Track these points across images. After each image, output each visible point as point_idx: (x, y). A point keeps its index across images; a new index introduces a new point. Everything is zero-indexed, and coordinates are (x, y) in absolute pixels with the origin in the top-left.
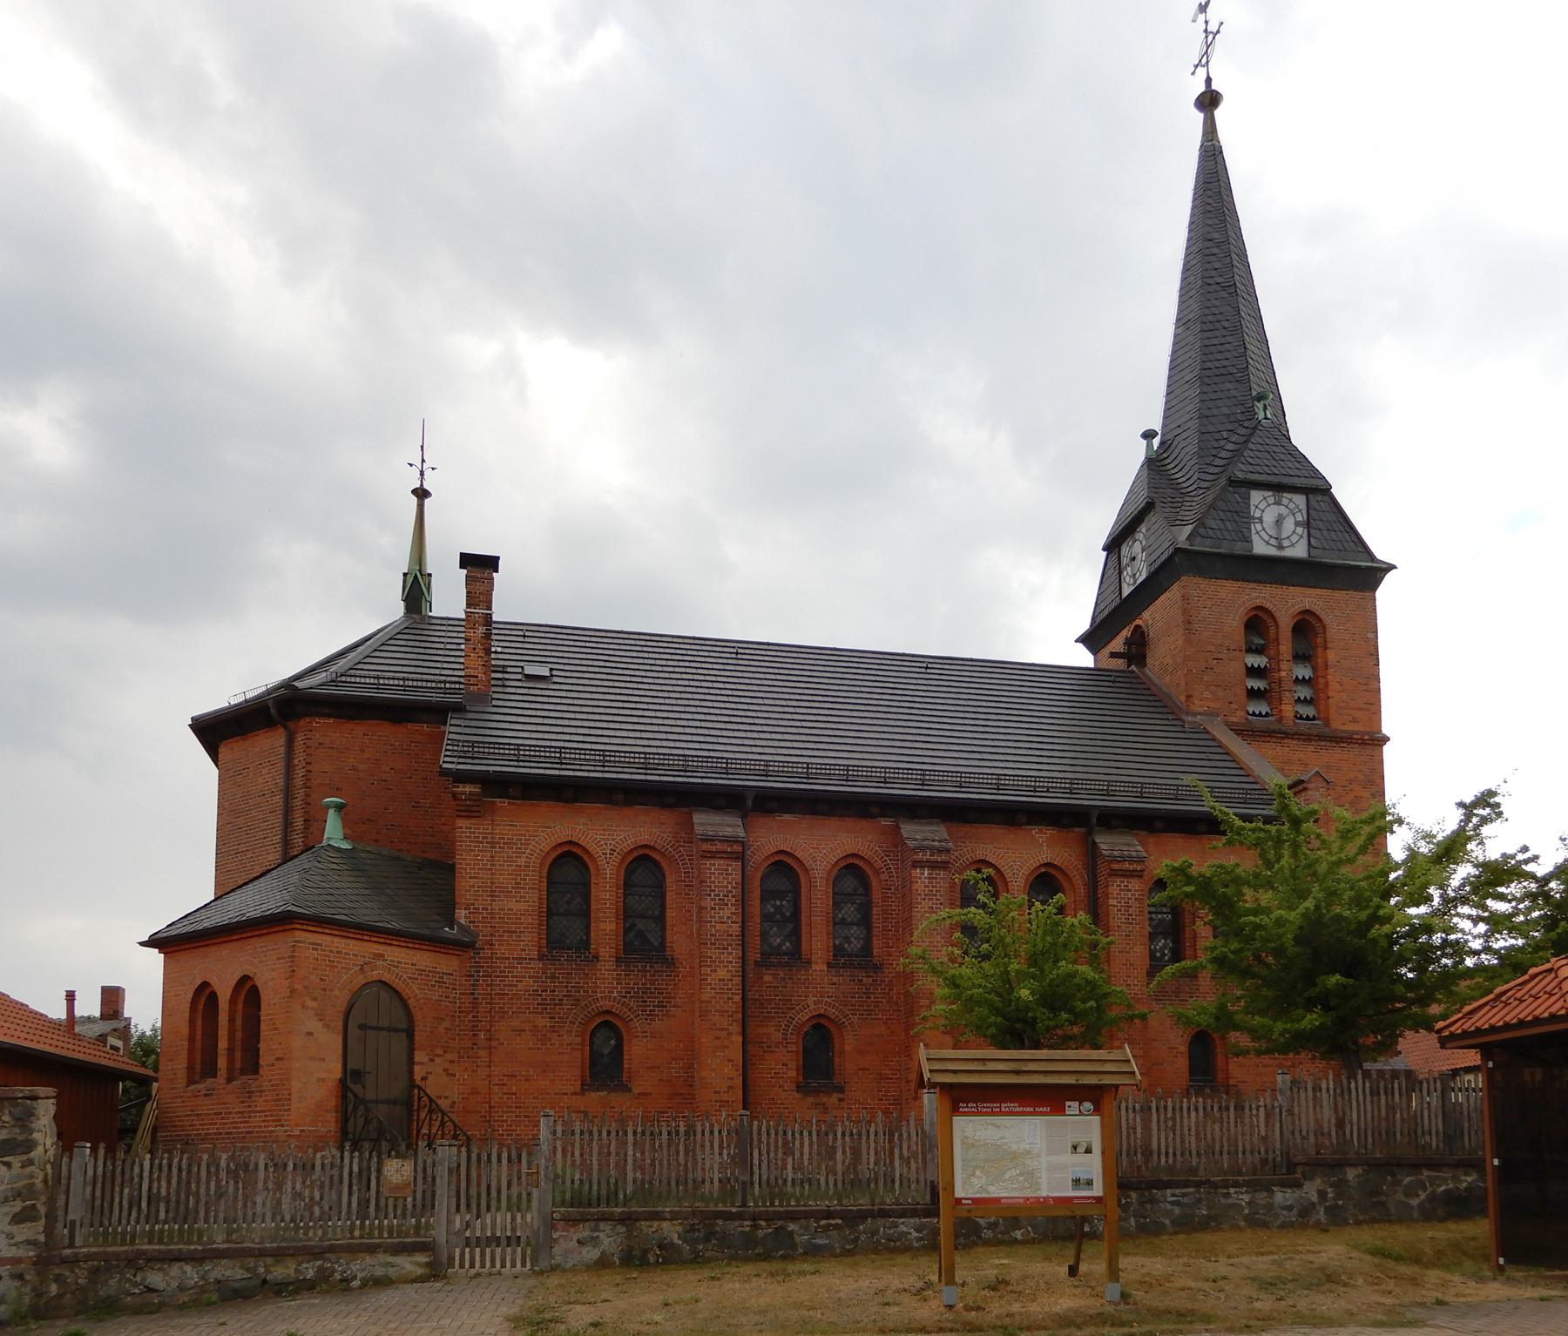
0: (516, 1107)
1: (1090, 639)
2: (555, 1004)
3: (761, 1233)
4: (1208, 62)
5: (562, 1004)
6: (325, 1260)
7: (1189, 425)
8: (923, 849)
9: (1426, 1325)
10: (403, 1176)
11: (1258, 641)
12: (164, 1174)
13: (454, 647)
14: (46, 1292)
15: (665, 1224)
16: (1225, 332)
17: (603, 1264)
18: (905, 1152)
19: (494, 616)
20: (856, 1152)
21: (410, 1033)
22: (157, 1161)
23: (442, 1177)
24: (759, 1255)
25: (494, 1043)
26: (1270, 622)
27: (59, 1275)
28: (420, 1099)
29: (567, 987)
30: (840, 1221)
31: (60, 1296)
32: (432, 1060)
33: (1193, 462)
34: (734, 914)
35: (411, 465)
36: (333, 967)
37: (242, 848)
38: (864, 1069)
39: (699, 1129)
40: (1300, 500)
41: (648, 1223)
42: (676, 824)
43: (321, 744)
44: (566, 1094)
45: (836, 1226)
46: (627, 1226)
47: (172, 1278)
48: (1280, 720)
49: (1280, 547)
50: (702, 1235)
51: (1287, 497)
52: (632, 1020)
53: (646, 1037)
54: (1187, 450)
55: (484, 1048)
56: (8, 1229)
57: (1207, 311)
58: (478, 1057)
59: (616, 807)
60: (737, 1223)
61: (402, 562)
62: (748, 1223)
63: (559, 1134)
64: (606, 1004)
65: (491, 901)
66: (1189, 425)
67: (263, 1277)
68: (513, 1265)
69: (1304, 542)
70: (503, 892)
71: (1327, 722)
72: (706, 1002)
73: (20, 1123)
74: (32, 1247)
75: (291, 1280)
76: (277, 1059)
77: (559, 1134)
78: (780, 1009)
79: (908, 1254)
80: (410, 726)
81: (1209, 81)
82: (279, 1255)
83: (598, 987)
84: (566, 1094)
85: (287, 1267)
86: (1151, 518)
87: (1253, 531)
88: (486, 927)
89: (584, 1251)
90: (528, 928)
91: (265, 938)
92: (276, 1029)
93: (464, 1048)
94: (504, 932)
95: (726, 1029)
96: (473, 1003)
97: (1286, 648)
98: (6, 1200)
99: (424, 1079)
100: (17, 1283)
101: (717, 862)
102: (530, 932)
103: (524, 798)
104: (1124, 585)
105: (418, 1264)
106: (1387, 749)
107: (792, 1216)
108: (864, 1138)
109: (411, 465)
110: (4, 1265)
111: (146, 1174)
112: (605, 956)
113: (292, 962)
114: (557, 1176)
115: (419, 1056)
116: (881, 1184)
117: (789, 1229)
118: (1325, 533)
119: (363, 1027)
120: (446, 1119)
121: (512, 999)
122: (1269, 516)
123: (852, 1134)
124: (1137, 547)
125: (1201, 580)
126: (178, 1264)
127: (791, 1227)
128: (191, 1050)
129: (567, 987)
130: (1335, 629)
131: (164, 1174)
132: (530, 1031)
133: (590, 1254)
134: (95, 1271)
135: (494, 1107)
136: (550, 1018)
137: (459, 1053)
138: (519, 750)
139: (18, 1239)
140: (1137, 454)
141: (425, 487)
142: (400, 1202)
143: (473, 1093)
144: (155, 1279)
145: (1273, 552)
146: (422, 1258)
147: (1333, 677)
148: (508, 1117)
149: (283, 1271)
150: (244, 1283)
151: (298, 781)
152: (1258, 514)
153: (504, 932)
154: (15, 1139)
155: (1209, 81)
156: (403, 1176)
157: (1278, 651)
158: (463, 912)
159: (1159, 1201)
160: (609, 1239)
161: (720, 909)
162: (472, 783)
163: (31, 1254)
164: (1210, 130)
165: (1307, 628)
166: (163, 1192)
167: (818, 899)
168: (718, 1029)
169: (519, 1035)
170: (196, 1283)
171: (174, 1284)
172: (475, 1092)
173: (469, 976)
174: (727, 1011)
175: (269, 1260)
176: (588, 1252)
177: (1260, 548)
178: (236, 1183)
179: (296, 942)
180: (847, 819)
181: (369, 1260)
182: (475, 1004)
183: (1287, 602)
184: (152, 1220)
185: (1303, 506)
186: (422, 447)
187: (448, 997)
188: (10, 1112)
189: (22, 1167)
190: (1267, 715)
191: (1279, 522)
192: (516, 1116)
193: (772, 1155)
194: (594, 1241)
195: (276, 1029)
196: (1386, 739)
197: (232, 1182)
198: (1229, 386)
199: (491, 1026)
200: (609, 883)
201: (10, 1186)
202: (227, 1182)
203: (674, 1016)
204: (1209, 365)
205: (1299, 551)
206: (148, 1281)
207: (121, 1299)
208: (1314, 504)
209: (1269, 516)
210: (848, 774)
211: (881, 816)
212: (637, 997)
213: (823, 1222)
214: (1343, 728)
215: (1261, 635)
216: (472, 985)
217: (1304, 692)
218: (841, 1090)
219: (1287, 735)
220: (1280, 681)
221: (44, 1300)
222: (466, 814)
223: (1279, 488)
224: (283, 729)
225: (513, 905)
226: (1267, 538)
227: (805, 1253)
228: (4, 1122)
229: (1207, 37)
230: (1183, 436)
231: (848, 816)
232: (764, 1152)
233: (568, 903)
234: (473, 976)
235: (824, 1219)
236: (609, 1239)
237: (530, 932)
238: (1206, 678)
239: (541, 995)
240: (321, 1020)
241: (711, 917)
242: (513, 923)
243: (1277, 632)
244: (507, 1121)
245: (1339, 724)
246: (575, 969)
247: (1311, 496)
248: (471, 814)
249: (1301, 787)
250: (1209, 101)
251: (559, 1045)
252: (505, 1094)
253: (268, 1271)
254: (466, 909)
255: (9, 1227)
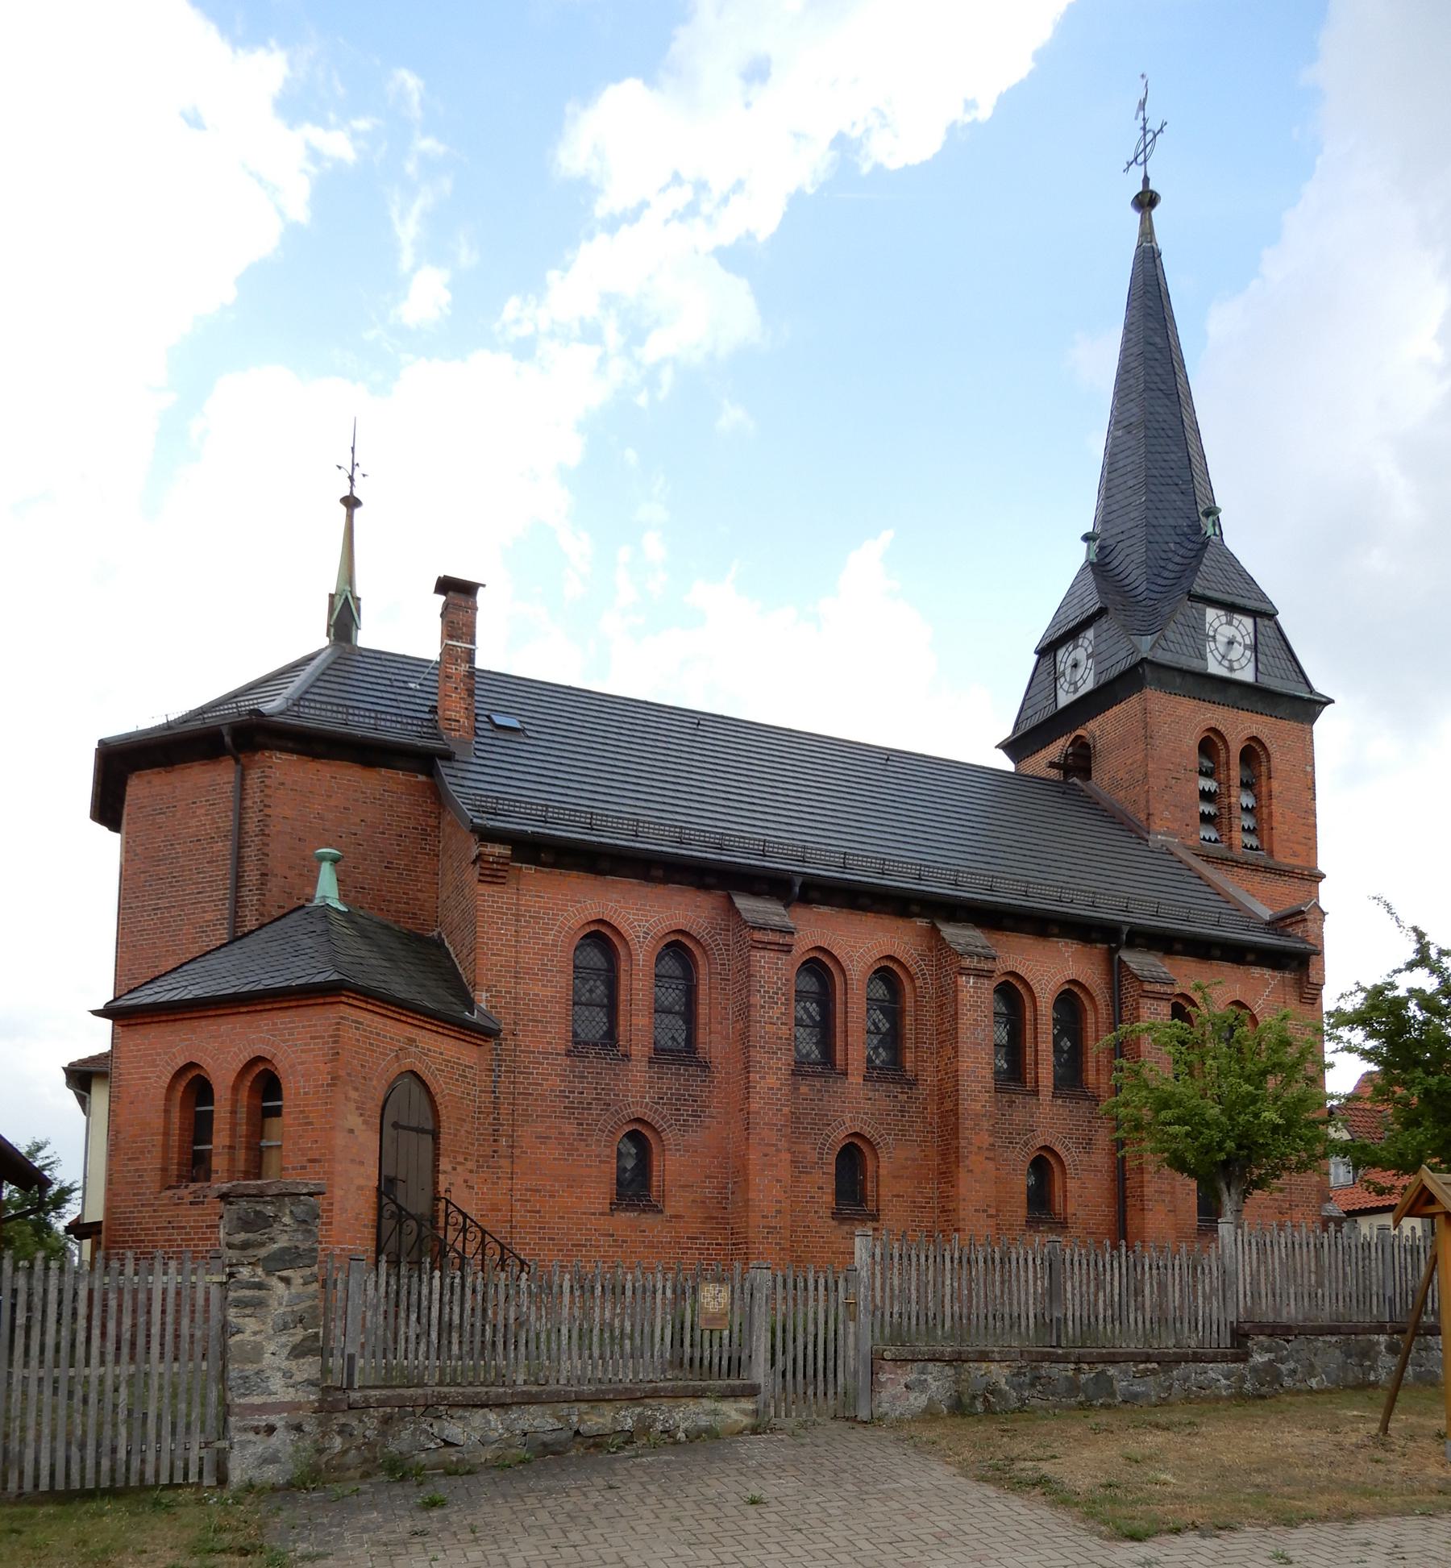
0: (540, 1228)
1: (1013, 747)
2: (583, 1109)
3: (1083, 1378)
4: (1145, 161)
5: (590, 1109)
6: (645, 1406)
7: (1134, 532)
8: (971, 955)
10: (720, 1304)
11: (1208, 764)
12: (457, 1297)
13: (402, 685)
14: (329, 1448)
15: (993, 1367)
16: (1169, 441)
17: (929, 1415)
18: (1207, 1288)
19: (478, 654)
20: (1162, 1286)
21: (435, 1135)
22: (448, 1280)
23: (760, 1307)
24: (1081, 1403)
25: (517, 1152)
27: (344, 1425)
28: (447, 1216)
29: (596, 1089)
30: (1155, 1365)
31: (344, 1452)
32: (454, 1169)
33: (1138, 572)
34: (784, 1014)
35: (340, 467)
36: (373, 1051)
37: (162, 903)
38: (898, 1196)
39: (1014, 1256)
40: (1248, 622)
41: (976, 1365)
42: (713, 908)
43: (283, 784)
44: (594, 1214)
45: (1153, 1372)
46: (955, 1368)
47: (474, 1429)
48: (1230, 847)
49: (1231, 669)
50: (1027, 1380)
51: (1238, 618)
52: (664, 1130)
53: (679, 1150)
54: (1133, 557)
55: (505, 1157)
56: (285, 1364)
57: (1151, 417)
58: (500, 1167)
59: (651, 884)
60: (1061, 1366)
61: (330, 583)
62: (1072, 1366)
63: (878, 1258)
64: (638, 1112)
65: (515, 983)
66: (1134, 532)
67: (575, 1428)
69: (1251, 665)
70: (528, 974)
71: (1271, 853)
72: (754, 1113)
73: (304, 1226)
74: (311, 1388)
75: (607, 1431)
76: (311, 1161)
77: (878, 1258)
78: (815, 1124)
80: (383, 771)
81: (1146, 180)
82: (596, 1400)
83: (629, 1091)
84: (594, 1214)
85: (603, 1415)
86: (1104, 624)
88: (509, 1013)
89: (912, 1396)
90: (554, 1017)
91: (290, 1013)
92: (310, 1123)
93: (482, 1156)
94: (529, 1020)
95: (773, 1145)
96: (494, 1103)
97: (1236, 773)
99: (448, 1191)
100: (294, 1436)
101: (766, 954)
102: (557, 1023)
103: (554, 865)
104: (1061, 693)
105: (744, 1412)
106: (1323, 886)
107: (1112, 1360)
108: (1170, 1271)
109: (340, 467)
110: (280, 1413)
111: (436, 1296)
112: (637, 1055)
113: (335, 1042)
115: (445, 1164)
116: (1186, 1325)
117: (1109, 1373)
118: (1271, 659)
119: (396, 1125)
120: (488, 1239)
121: (536, 1100)
123: (1158, 1268)
124: (1080, 654)
125: (1162, 695)
126: (481, 1412)
127: (1112, 1371)
128: (166, 1147)
129: (596, 1089)
130: (1280, 759)
131: (457, 1297)
132: (556, 1138)
133: (918, 1401)
134: (387, 1420)
135: (516, 1227)
136: (578, 1124)
137: (478, 1161)
138: (547, 811)
139: (298, 1378)
140: (1077, 555)
141: (356, 494)
142: (716, 1335)
143: (492, 1210)
144: (454, 1430)
145: (1224, 672)
146: (747, 1405)
147: (1276, 808)
148: (531, 1239)
149: (598, 1420)
150: (554, 1435)
151: (251, 827)
152: (1211, 633)
153: (529, 1020)
154: (297, 1247)
155: (1146, 180)
156: (720, 1304)
157: (1228, 775)
158: (484, 994)
159: (1433, 1349)
160: (937, 1383)
161: (769, 1008)
162: (502, 843)
163: (312, 1397)
164: (1147, 232)
165: (1253, 753)
166: (456, 1320)
167: (855, 1003)
168: (767, 1145)
169: (544, 1143)
170: (501, 1435)
171: (476, 1437)
172: (495, 1208)
173: (490, 1070)
174: (776, 1125)
175: (584, 1407)
176: (915, 1399)
177: (1214, 668)
178: (539, 1309)
179: (342, 1018)
180: (883, 916)
181: (692, 1406)
182: (496, 1105)
183: (1239, 726)
184: (444, 1355)
185: (1251, 628)
186: (353, 449)
187: (468, 1094)
188: (291, 1212)
189: (305, 1284)
190: (1216, 841)
192: (540, 1239)
193: (1084, 1288)
194: (922, 1385)
195: (310, 1123)
196: (1322, 876)
197: (533, 1308)
198: (1174, 496)
199: (513, 1131)
200: (642, 970)
201: (289, 1309)
202: (529, 1308)
203: (709, 1128)
204: (1155, 472)
205: (1247, 675)
206: (446, 1432)
207: (413, 1456)
208: (1260, 627)
211: (919, 916)
212: (671, 1104)
213: (1142, 1366)
214: (1286, 861)
215: (1210, 758)
216: (494, 1082)
217: (1248, 822)
218: (875, 1218)
219: (1237, 864)
220: (1230, 808)
221: (325, 1458)
222: (489, 879)
223: (1231, 608)
224: (233, 762)
225: (537, 989)
227: (1125, 1402)
228: (285, 1225)
229: (1145, 135)
230: (1127, 543)
231: (886, 913)
232: (1077, 1284)
233: (591, 991)
234: (494, 1071)
235: (1142, 1362)
236: (937, 1383)
237: (557, 1023)
238: (1166, 797)
239: (568, 1097)
240: (361, 1115)
241: (761, 1016)
242: (538, 1011)
243: (1228, 757)
244: (529, 1244)
245: (1283, 858)
246: (606, 1069)
247: (1258, 619)
248: (495, 880)
249: (1299, 918)
250: (1146, 201)
251: (587, 1156)
252: (529, 1212)
253: (581, 1421)
254: (487, 991)
255: (287, 1363)
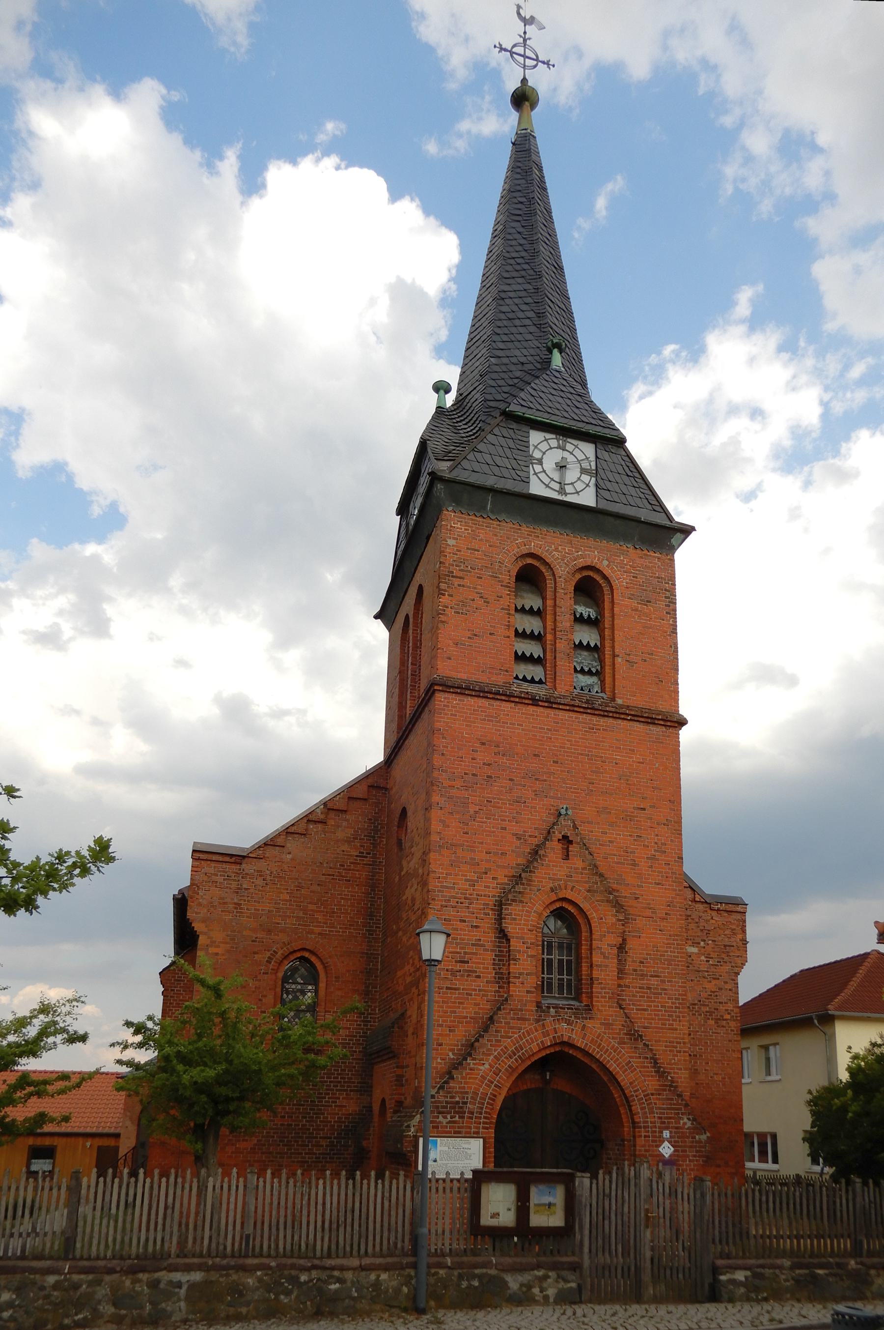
9: (561, 353)
26: (547, 574)
40: (588, 449)
49: (562, 491)
68: (746, 1191)
69: (592, 490)
79: (30, 1080)
87: (532, 472)
98: (128, 1024)
114: (634, 1165)
122: (550, 461)
177: (536, 488)
191: (562, 467)
205: (588, 498)
209: (550, 461)
210: (298, 816)
217: (585, 660)
226: (546, 480)
